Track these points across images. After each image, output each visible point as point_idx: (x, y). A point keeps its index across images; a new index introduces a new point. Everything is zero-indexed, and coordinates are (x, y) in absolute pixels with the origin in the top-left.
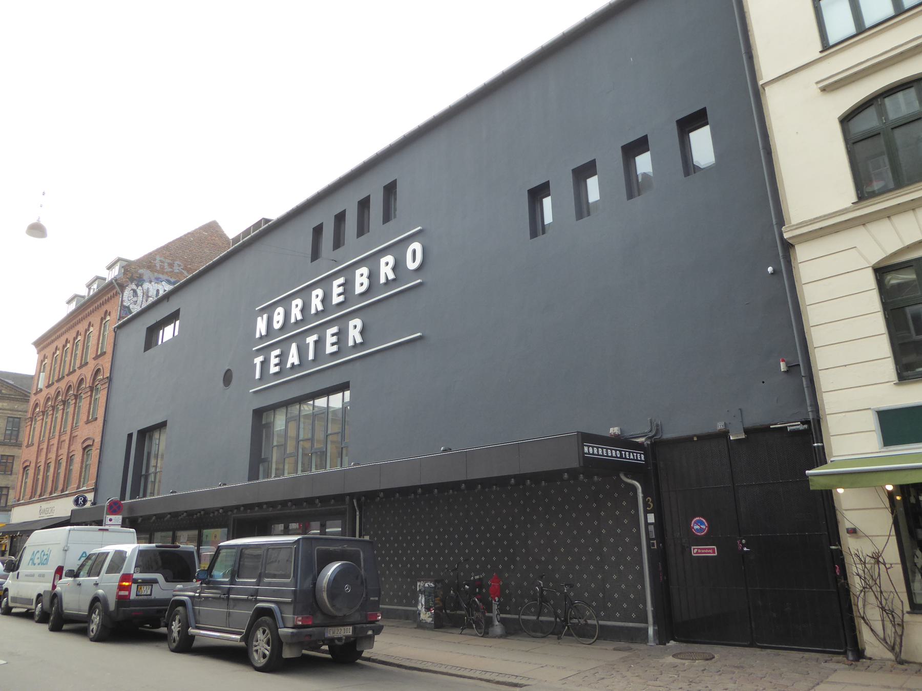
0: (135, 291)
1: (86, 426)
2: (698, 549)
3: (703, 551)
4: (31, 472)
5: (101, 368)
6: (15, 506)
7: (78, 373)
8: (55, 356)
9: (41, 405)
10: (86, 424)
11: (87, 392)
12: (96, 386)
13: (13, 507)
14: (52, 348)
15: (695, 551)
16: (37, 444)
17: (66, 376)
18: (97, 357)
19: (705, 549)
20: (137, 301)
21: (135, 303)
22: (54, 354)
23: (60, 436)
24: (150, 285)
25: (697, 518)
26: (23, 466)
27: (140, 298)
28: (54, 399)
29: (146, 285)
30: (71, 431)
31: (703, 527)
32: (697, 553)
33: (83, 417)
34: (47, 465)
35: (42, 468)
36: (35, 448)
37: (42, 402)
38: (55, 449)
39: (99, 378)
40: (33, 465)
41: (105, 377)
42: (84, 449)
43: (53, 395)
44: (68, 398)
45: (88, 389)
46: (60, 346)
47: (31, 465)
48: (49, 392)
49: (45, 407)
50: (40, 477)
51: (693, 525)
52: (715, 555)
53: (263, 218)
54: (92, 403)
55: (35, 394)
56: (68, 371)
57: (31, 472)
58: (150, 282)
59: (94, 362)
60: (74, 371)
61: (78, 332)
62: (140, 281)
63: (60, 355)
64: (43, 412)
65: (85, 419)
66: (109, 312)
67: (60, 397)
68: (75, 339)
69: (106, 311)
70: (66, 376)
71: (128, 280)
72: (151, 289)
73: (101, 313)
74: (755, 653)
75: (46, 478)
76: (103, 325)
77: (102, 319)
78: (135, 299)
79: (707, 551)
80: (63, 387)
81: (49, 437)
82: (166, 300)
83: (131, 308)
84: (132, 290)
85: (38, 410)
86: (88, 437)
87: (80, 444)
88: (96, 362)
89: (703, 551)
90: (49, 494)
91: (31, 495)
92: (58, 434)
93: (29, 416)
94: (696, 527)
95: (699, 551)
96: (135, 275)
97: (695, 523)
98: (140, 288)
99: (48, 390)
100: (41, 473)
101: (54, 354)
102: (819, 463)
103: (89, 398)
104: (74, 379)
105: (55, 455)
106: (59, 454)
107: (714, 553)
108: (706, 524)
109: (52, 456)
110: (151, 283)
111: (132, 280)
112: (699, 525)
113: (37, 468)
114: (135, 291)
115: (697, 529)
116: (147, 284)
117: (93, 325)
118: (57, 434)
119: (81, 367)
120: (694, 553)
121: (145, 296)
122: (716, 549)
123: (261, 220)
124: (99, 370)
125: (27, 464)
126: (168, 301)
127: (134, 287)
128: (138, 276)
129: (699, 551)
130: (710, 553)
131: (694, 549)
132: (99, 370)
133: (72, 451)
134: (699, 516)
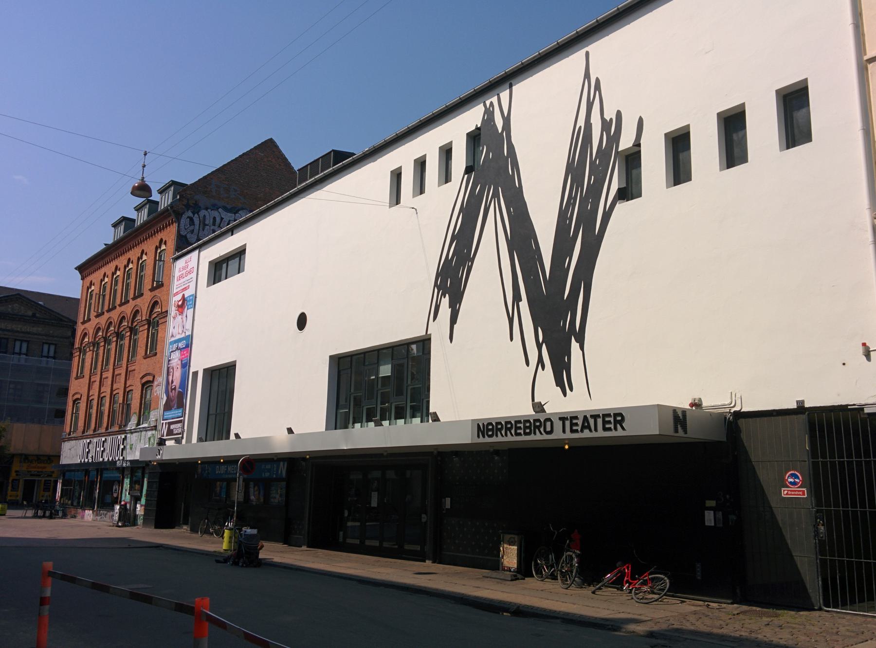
0: (191, 219)
1: (145, 361)
2: (788, 490)
3: (793, 493)
4: (83, 405)
5: (159, 301)
6: (66, 441)
7: (132, 303)
8: (103, 283)
9: (91, 336)
10: (145, 359)
11: (144, 325)
12: (153, 320)
13: (64, 441)
14: (98, 275)
15: (786, 492)
16: (88, 377)
17: (118, 307)
18: (152, 289)
19: (798, 495)
20: (193, 230)
21: (192, 231)
22: (102, 281)
23: (114, 370)
24: (206, 212)
25: (792, 472)
26: (72, 399)
27: (197, 227)
28: (105, 331)
29: (203, 213)
30: (127, 365)
31: (797, 480)
32: (787, 494)
33: (141, 351)
34: (101, 399)
35: (95, 403)
36: (86, 380)
37: (91, 332)
38: (110, 382)
39: (157, 310)
40: (84, 398)
41: (163, 311)
42: (143, 385)
43: (103, 326)
44: (121, 330)
45: (145, 322)
46: (109, 273)
47: (82, 398)
48: (99, 321)
49: (95, 338)
50: (94, 411)
51: (788, 478)
52: (804, 497)
53: (333, 151)
54: (150, 337)
55: (84, 323)
56: (119, 302)
57: (83, 405)
58: (207, 209)
59: (150, 293)
60: (103, 313)
61: (129, 259)
62: (196, 209)
63: (110, 283)
64: (95, 344)
65: (143, 354)
66: (164, 241)
67: (112, 328)
68: (113, 274)
69: (162, 240)
70: (118, 307)
71: (183, 207)
72: (207, 217)
73: (155, 241)
74: (845, 617)
75: (100, 414)
76: (158, 254)
77: (157, 248)
78: (192, 228)
79: (797, 493)
80: (114, 318)
81: (102, 369)
82: (230, 233)
83: (188, 237)
84: (188, 217)
85: (86, 340)
86: (148, 372)
87: (139, 380)
88: (154, 293)
89: (793, 493)
90: (105, 430)
91: (84, 430)
92: (112, 367)
93: (77, 347)
94: (791, 480)
95: (789, 493)
96: (191, 202)
97: (788, 476)
98: (196, 215)
99: (97, 320)
100: (95, 407)
101: (102, 281)
102: (790, 145)
103: (146, 331)
104: (128, 309)
105: (110, 388)
106: (114, 388)
107: (804, 494)
108: (800, 478)
109: (106, 389)
110: (207, 210)
111: (188, 207)
112: (793, 479)
113: (89, 402)
114: (191, 219)
115: (791, 482)
116: (204, 211)
117: (94, 283)
118: (111, 367)
119: (109, 311)
120: (784, 495)
121: (201, 226)
122: (806, 491)
123: (331, 152)
124: (137, 311)
125: (78, 396)
126: (232, 235)
127: (190, 214)
128: (194, 202)
129: (789, 493)
130: (800, 495)
131: (784, 491)
132: (137, 311)
133: (130, 386)
134: (793, 470)
